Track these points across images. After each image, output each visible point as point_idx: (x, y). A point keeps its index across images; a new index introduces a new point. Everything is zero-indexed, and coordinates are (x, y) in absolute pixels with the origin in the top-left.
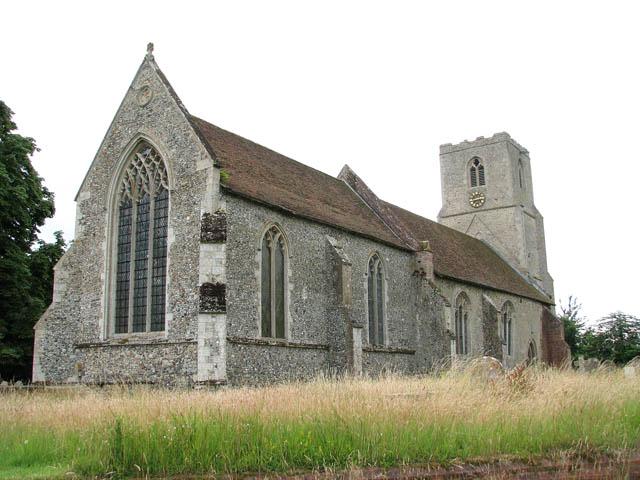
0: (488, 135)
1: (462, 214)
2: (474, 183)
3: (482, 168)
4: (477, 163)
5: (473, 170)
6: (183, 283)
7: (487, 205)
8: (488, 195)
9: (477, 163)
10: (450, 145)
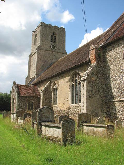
1: (47, 50)
2: (52, 41)
3: (55, 37)
4: (53, 34)
5: (52, 36)
7: (57, 50)
9: (53, 34)
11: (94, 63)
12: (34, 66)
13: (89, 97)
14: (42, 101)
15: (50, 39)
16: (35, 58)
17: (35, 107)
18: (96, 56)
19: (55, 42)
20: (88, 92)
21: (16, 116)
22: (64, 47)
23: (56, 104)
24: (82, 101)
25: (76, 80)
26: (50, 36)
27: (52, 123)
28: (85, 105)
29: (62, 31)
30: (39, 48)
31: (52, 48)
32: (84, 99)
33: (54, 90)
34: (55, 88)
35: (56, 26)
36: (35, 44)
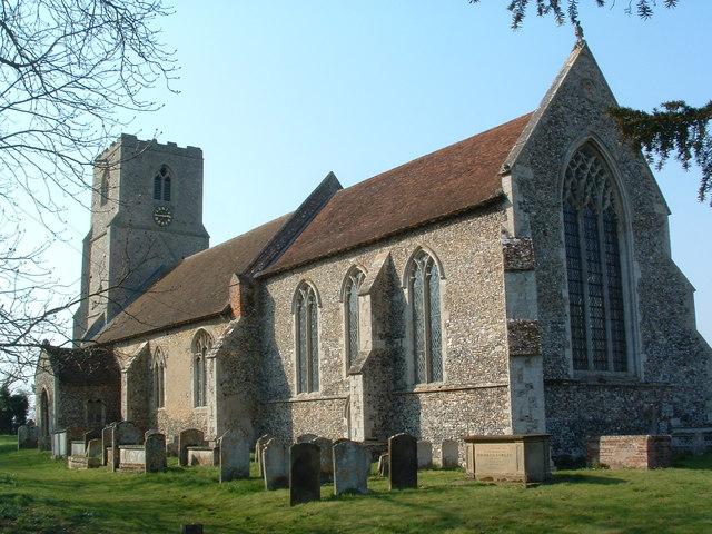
0: (182, 144)
2: (157, 196)
3: (168, 180)
4: (163, 171)
5: (158, 178)
6: (654, 323)
8: (175, 215)
9: (163, 171)
10: (134, 137)
11: (237, 312)
12: (101, 280)
13: (223, 396)
14: (124, 399)
15: (151, 190)
16: (103, 248)
17: (108, 412)
18: (241, 302)
19: (167, 198)
20: (220, 383)
21: (67, 437)
22: (199, 214)
23: (162, 406)
24: (209, 403)
25: (205, 349)
26: (152, 182)
27: (40, 469)
28: (215, 413)
29: (193, 157)
30: (116, 223)
31: (160, 218)
32: (212, 398)
33: (157, 367)
34: (159, 363)
35: (172, 145)
36: (105, 199)
